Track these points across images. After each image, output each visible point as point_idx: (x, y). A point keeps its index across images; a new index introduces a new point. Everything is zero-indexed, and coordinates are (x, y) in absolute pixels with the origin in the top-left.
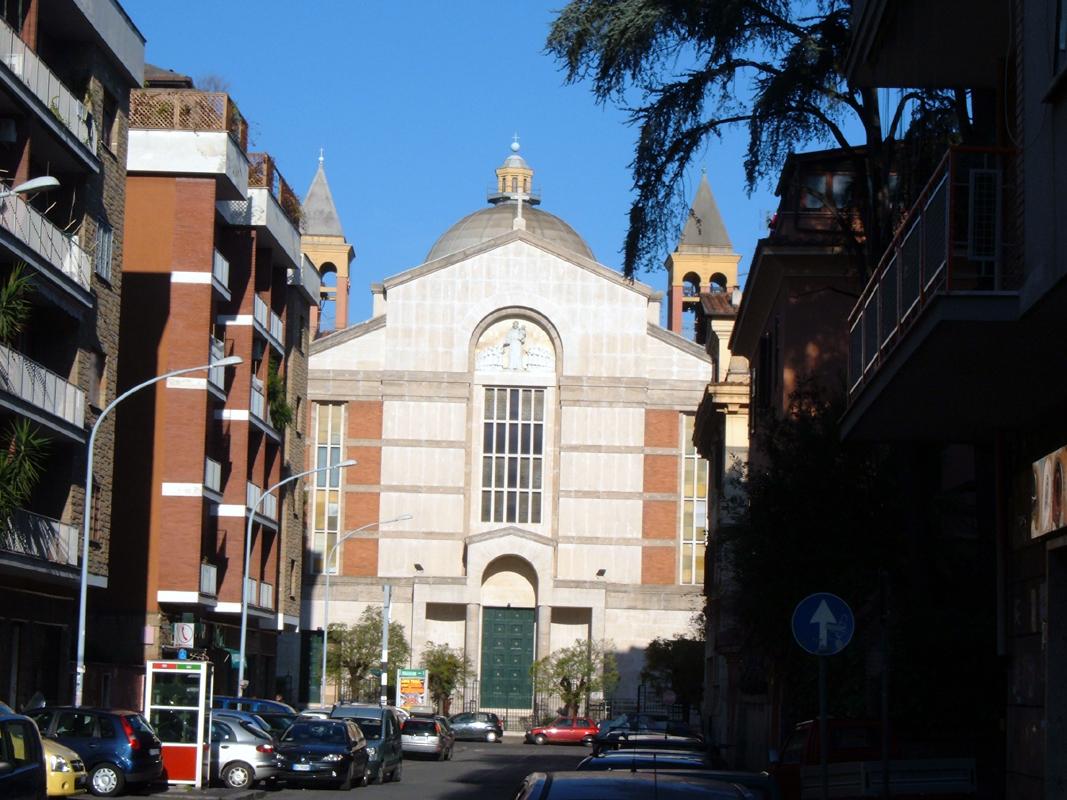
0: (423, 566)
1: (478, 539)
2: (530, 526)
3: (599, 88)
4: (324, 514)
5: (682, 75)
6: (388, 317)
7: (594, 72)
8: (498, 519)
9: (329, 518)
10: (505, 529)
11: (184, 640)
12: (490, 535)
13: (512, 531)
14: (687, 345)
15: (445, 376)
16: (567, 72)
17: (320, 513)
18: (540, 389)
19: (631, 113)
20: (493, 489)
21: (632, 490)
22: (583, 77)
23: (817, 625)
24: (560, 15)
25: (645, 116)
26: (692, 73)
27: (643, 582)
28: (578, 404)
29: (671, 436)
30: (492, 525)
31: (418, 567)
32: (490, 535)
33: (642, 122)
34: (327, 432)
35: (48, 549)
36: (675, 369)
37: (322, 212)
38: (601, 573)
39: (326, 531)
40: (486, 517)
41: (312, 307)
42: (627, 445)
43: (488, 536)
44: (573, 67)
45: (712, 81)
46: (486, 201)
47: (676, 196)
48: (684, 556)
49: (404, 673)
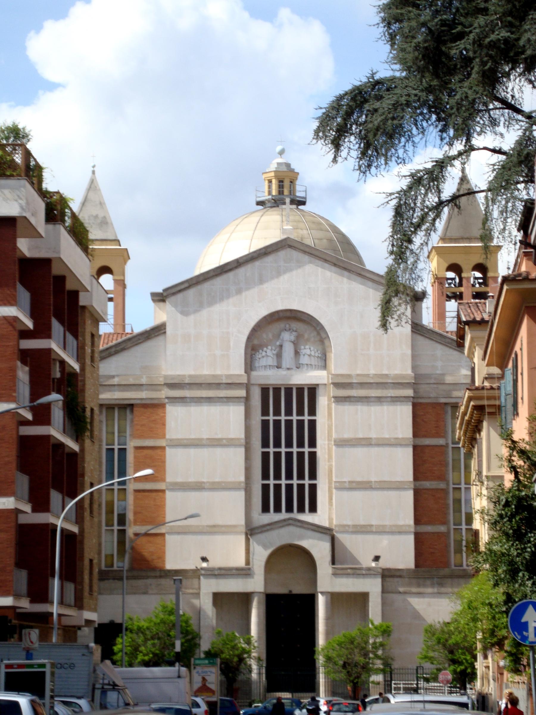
0: (208, 558)
1: (260, 530)
2: (307, 517)
3: (360, 167)
4: (113, 512)
5: (425, 162)
6: (167, 324)
7: (355, 154)
8: (278, 509)
9: (119, 515)
10: (284, 520)
11: (30, 644)
12: (271, 526)
13: (291, 522)
14: (450, 341)
15: (224, 378)
16: (331, 156)
17: (110, 511)
18: (313, 390)
19: (384, 195)
20: (272, 482)
21: (402, 480)
22: (346, 159)
23: (526, 623)
24: (324, 111)
25: (397, 197)
26: (435, 159)
27: (417, 565)
28: (348, 399)
29: (436, 427)
30: (272, 517)
31: (204, 559)
32: (271, 526)
33: (394, 202)
34: (113, 433)
35: (260, 674)
36: (439, 364)
37: (96, 217)
38: (377, 558)
39: (116, 527)
40: (265, 509)
41: (100, 323)
42: (396, 436)
43: (268, 527)
44: (337, 145)
45: (452, 165)
46: (255, 203)
47: (423, 263)
48: (455, 541)
49: (198, 662)
